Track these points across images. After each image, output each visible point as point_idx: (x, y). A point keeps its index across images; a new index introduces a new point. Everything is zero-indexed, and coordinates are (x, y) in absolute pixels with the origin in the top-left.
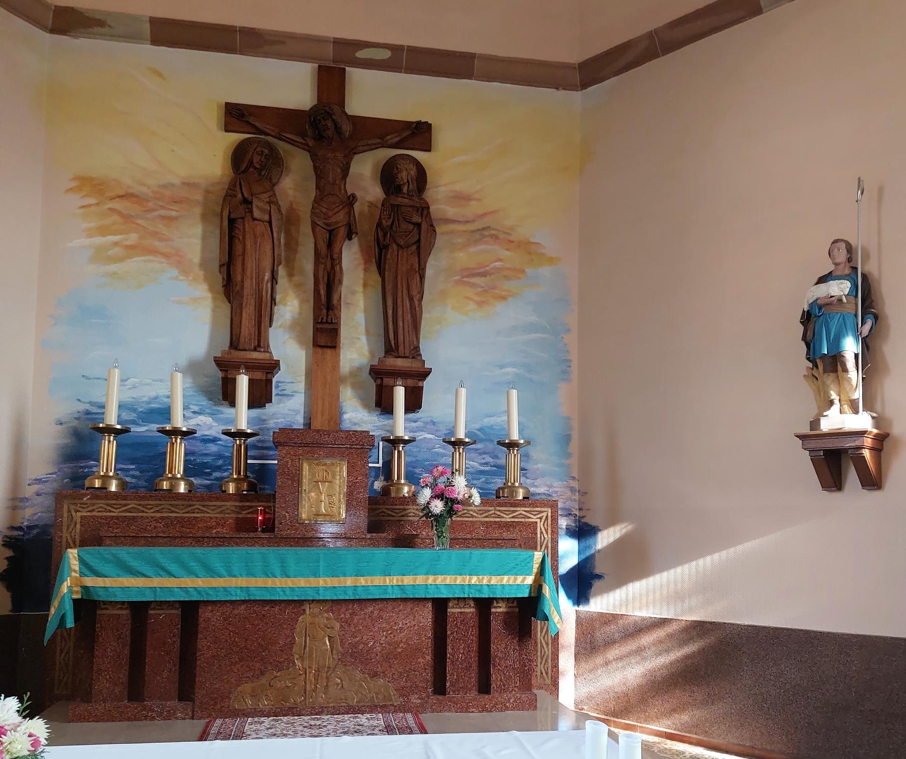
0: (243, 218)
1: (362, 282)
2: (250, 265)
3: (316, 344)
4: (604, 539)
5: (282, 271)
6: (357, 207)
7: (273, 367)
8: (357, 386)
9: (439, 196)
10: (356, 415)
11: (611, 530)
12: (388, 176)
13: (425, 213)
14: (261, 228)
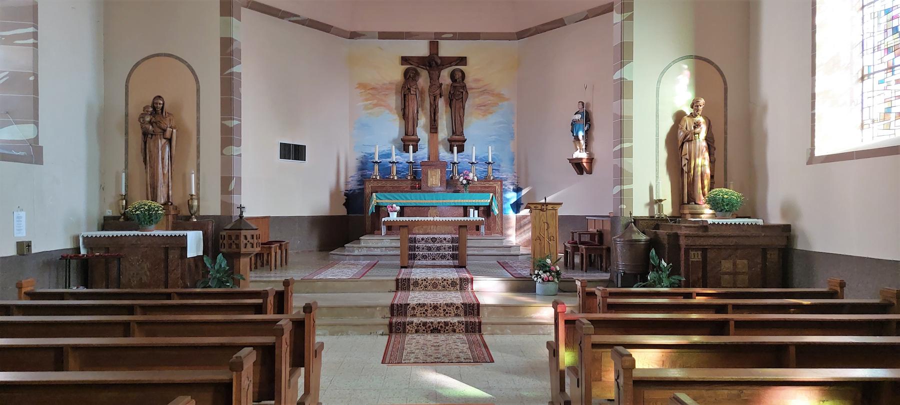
4: (524, 192)
9: (469, 82)
10: (444, 154)
11: (15, 127)
12: (452, 76)
14: (413, 96)
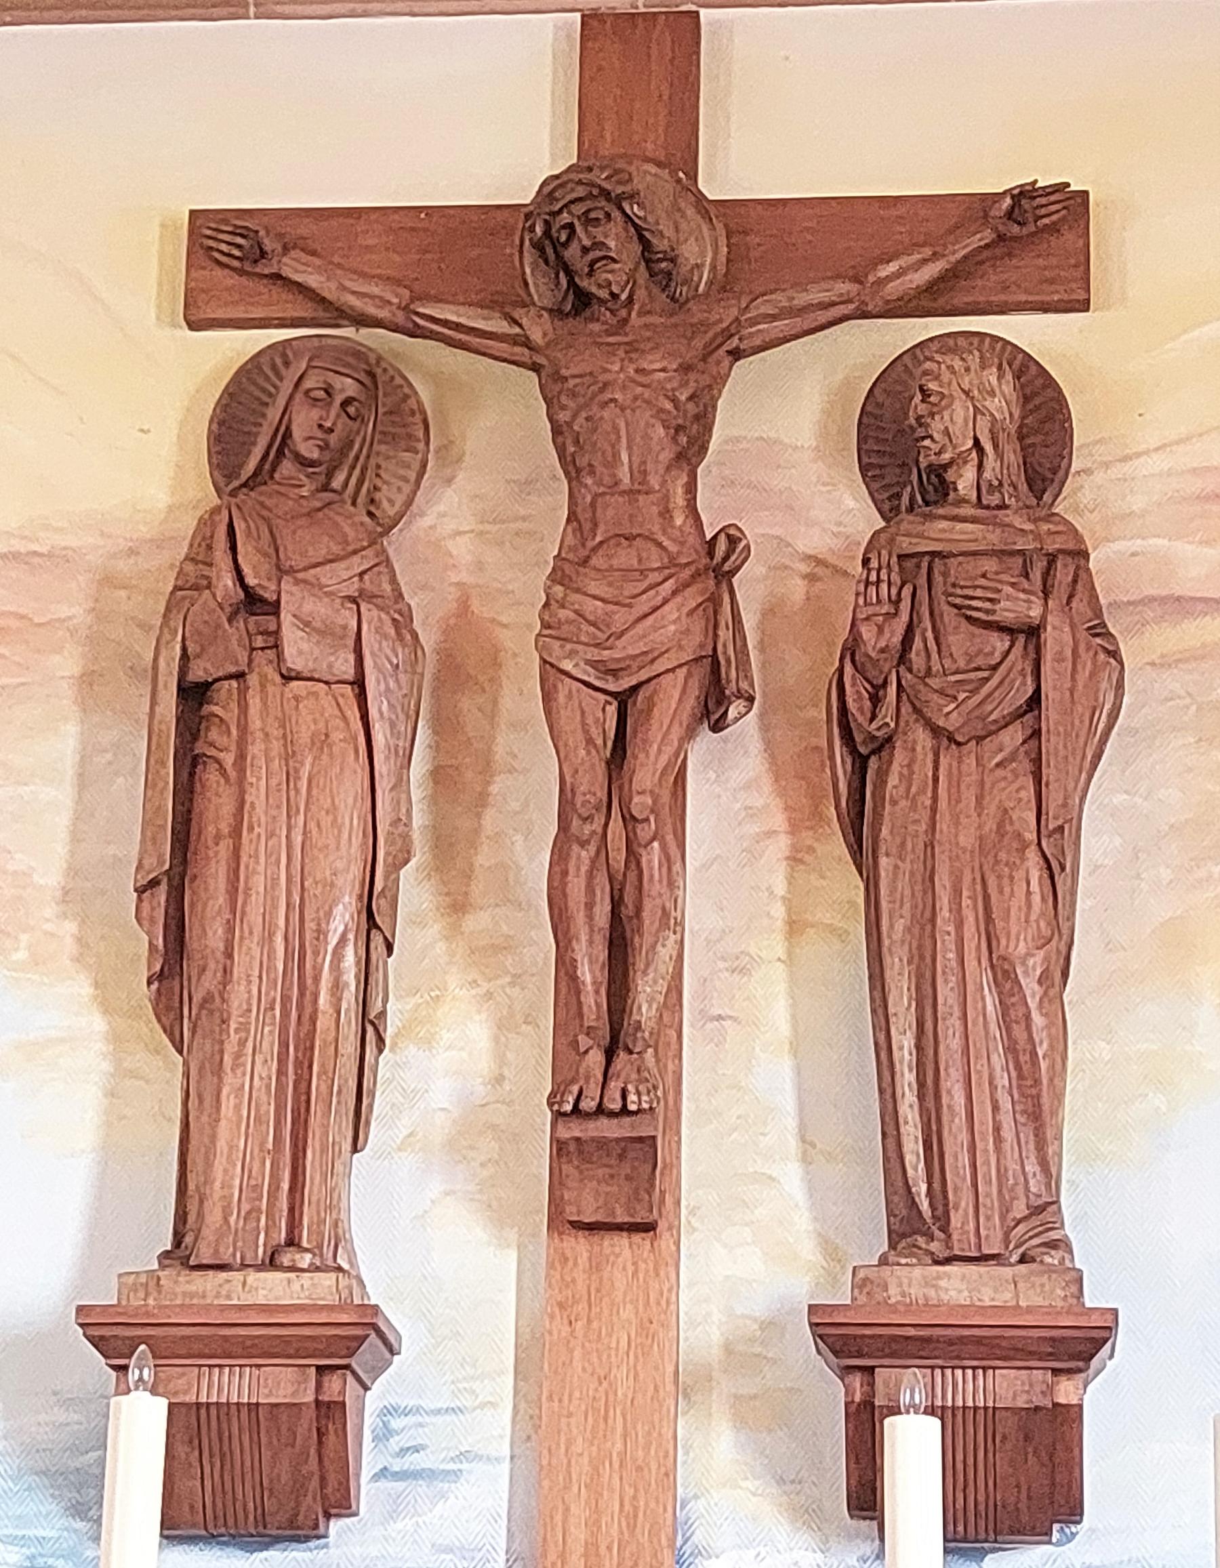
0: (239, 676)
1: (779, 911)
2: (265, 875)
3: (564, 1222)
5: (414, 893)
6: (751, 588)
7: (348, 1343)
8: (758, 1415)
12: (892, 444)
13: (1063, 573)
14: (322, 710)
